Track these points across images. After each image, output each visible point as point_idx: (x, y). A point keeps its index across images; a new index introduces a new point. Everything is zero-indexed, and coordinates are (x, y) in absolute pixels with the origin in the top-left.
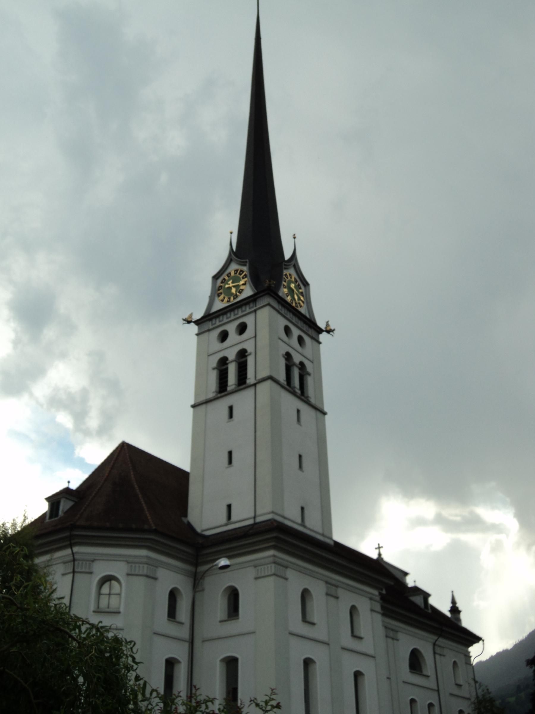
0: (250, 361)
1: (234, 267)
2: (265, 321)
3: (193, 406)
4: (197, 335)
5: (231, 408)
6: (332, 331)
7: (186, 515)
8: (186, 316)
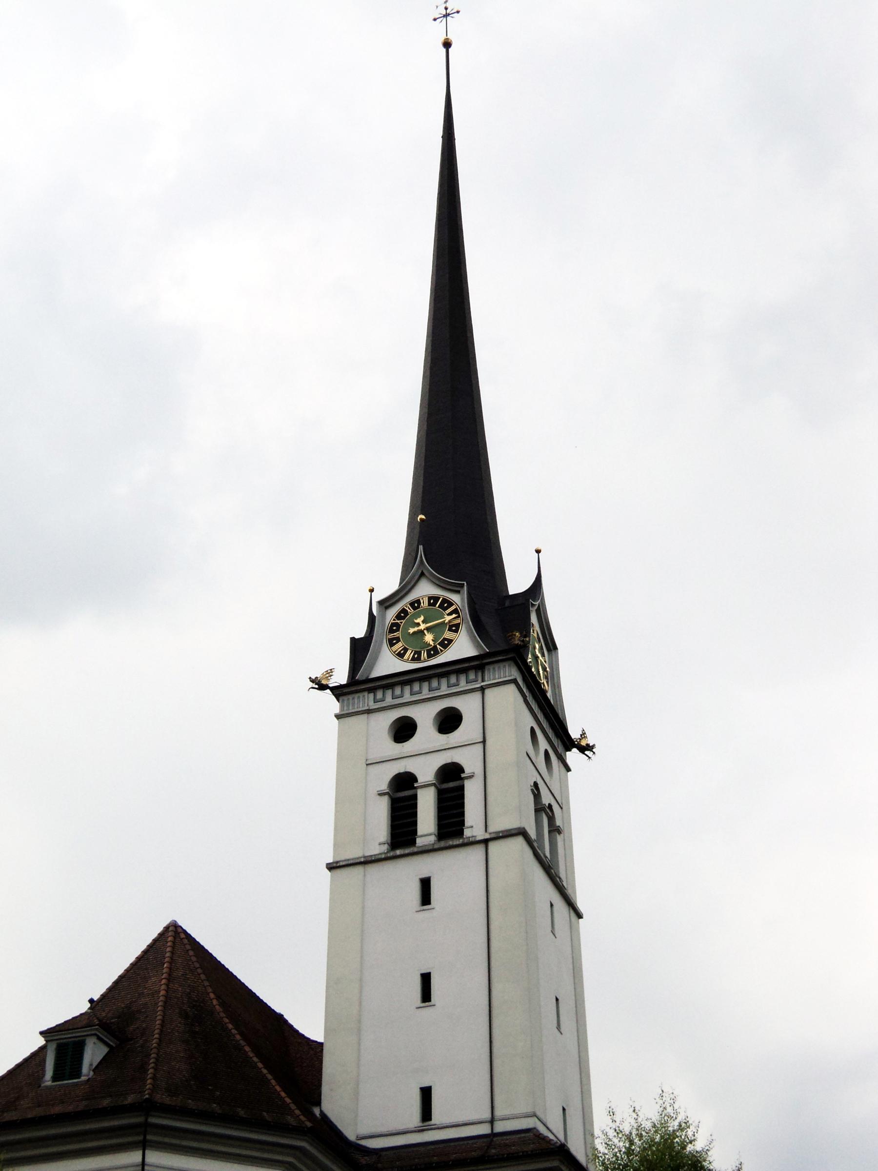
1: (425, 590)
2: (499, 711)
3: (331, 867)
4: (338, 717)
5: (426, 885)
7: (318, 1103)
8: (317, 674)
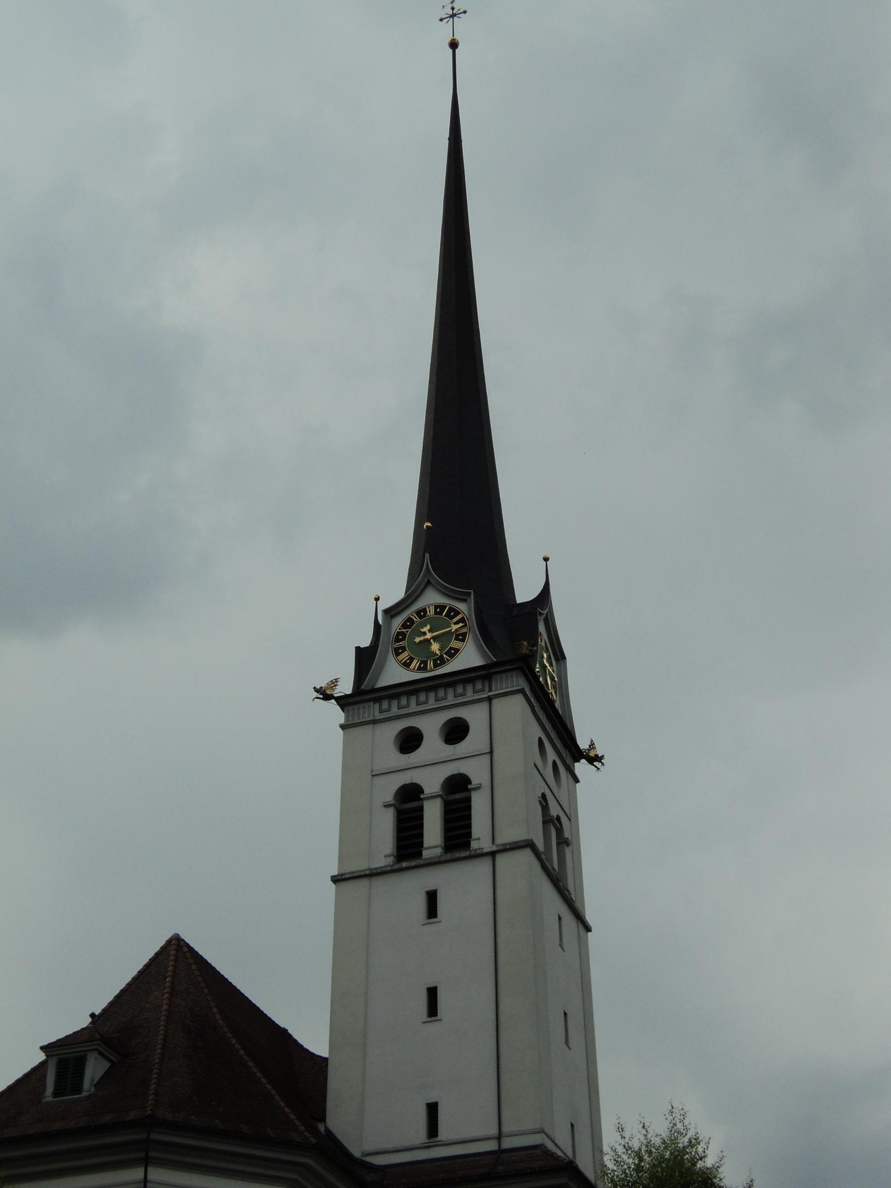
0: (479, 804)
1: (431, 598)
3: (336, 880)
4: (343, 727)
5: (432, 898)
6: (599, 759)
7: (323, 1119)
8: (322, 683)
